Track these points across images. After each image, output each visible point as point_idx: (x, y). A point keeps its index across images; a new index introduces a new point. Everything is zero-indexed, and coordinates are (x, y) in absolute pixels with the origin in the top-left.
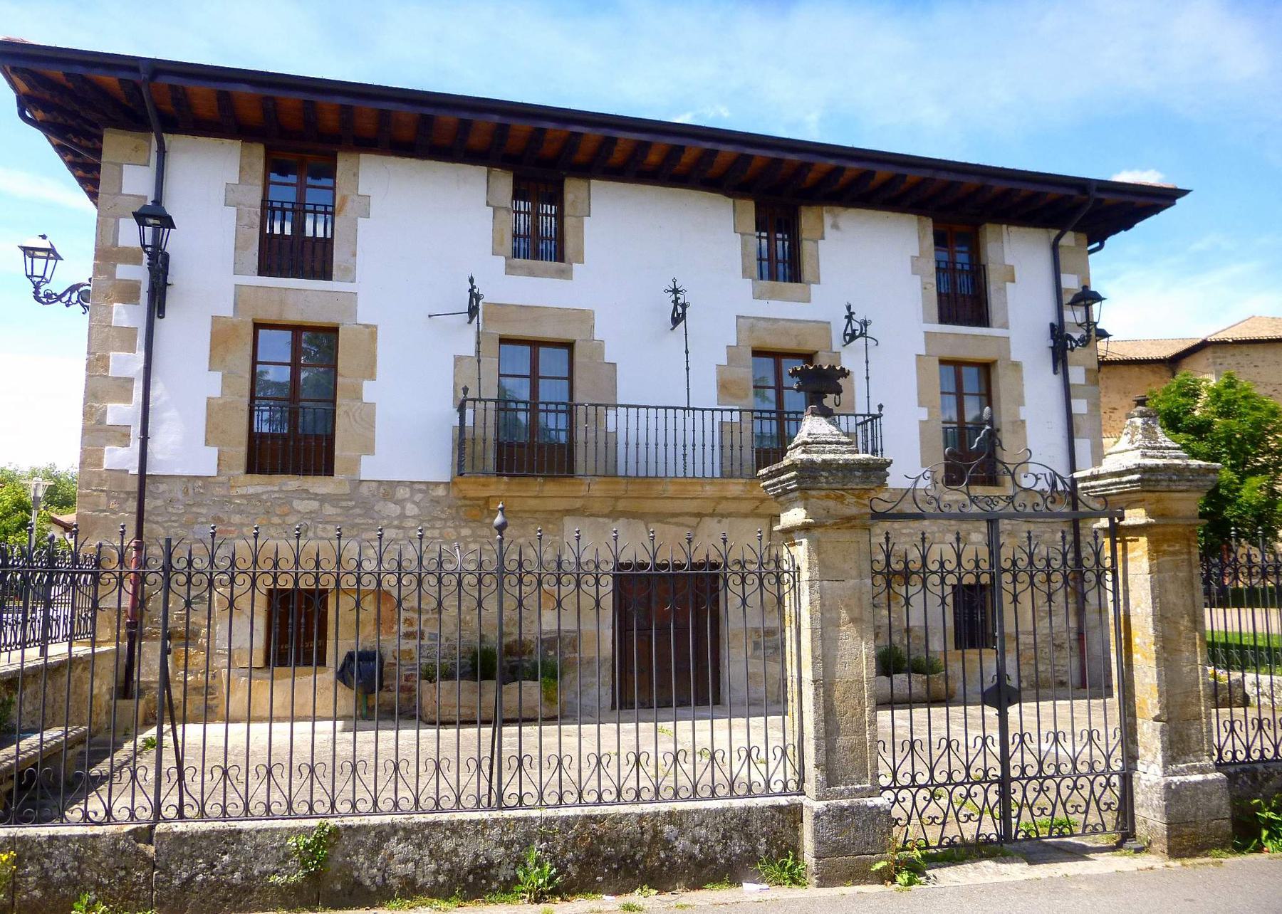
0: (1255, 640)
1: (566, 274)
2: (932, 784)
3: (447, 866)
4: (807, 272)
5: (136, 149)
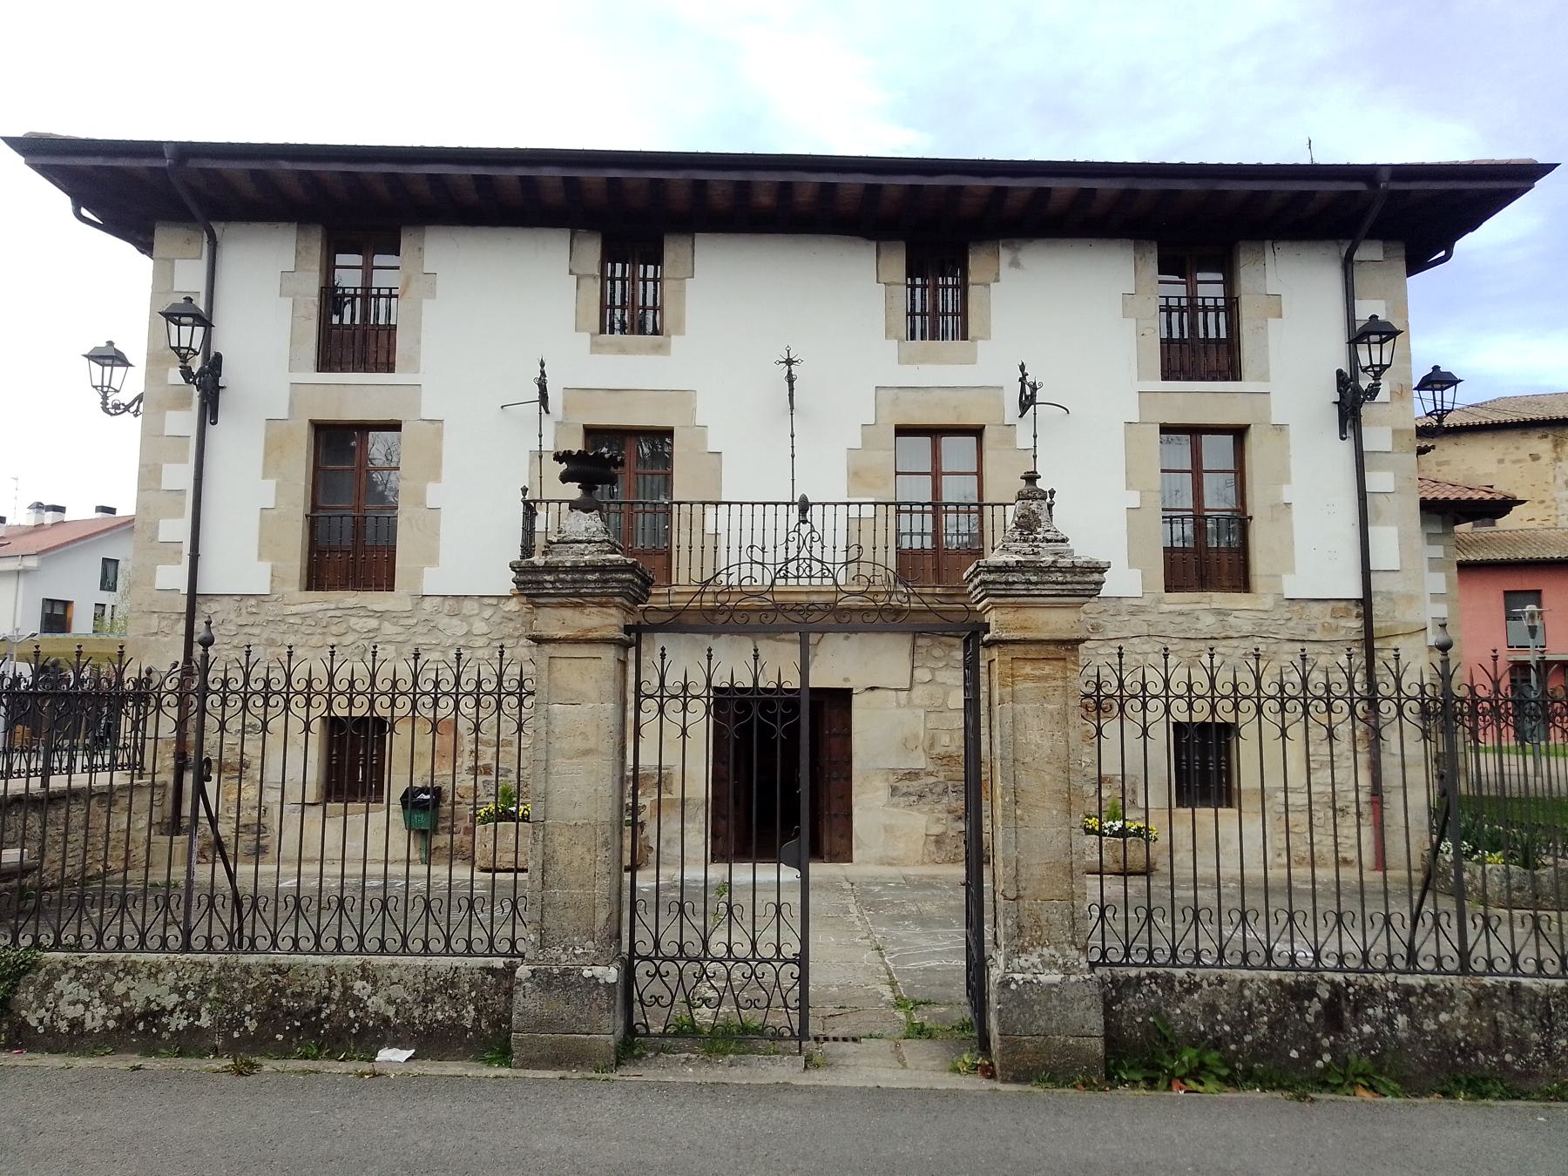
0: (1480, 790)
1: (661, 349)
2: (755, 957)
3: (118, 1011)
4: (972, 330)
5: (189, 241)
